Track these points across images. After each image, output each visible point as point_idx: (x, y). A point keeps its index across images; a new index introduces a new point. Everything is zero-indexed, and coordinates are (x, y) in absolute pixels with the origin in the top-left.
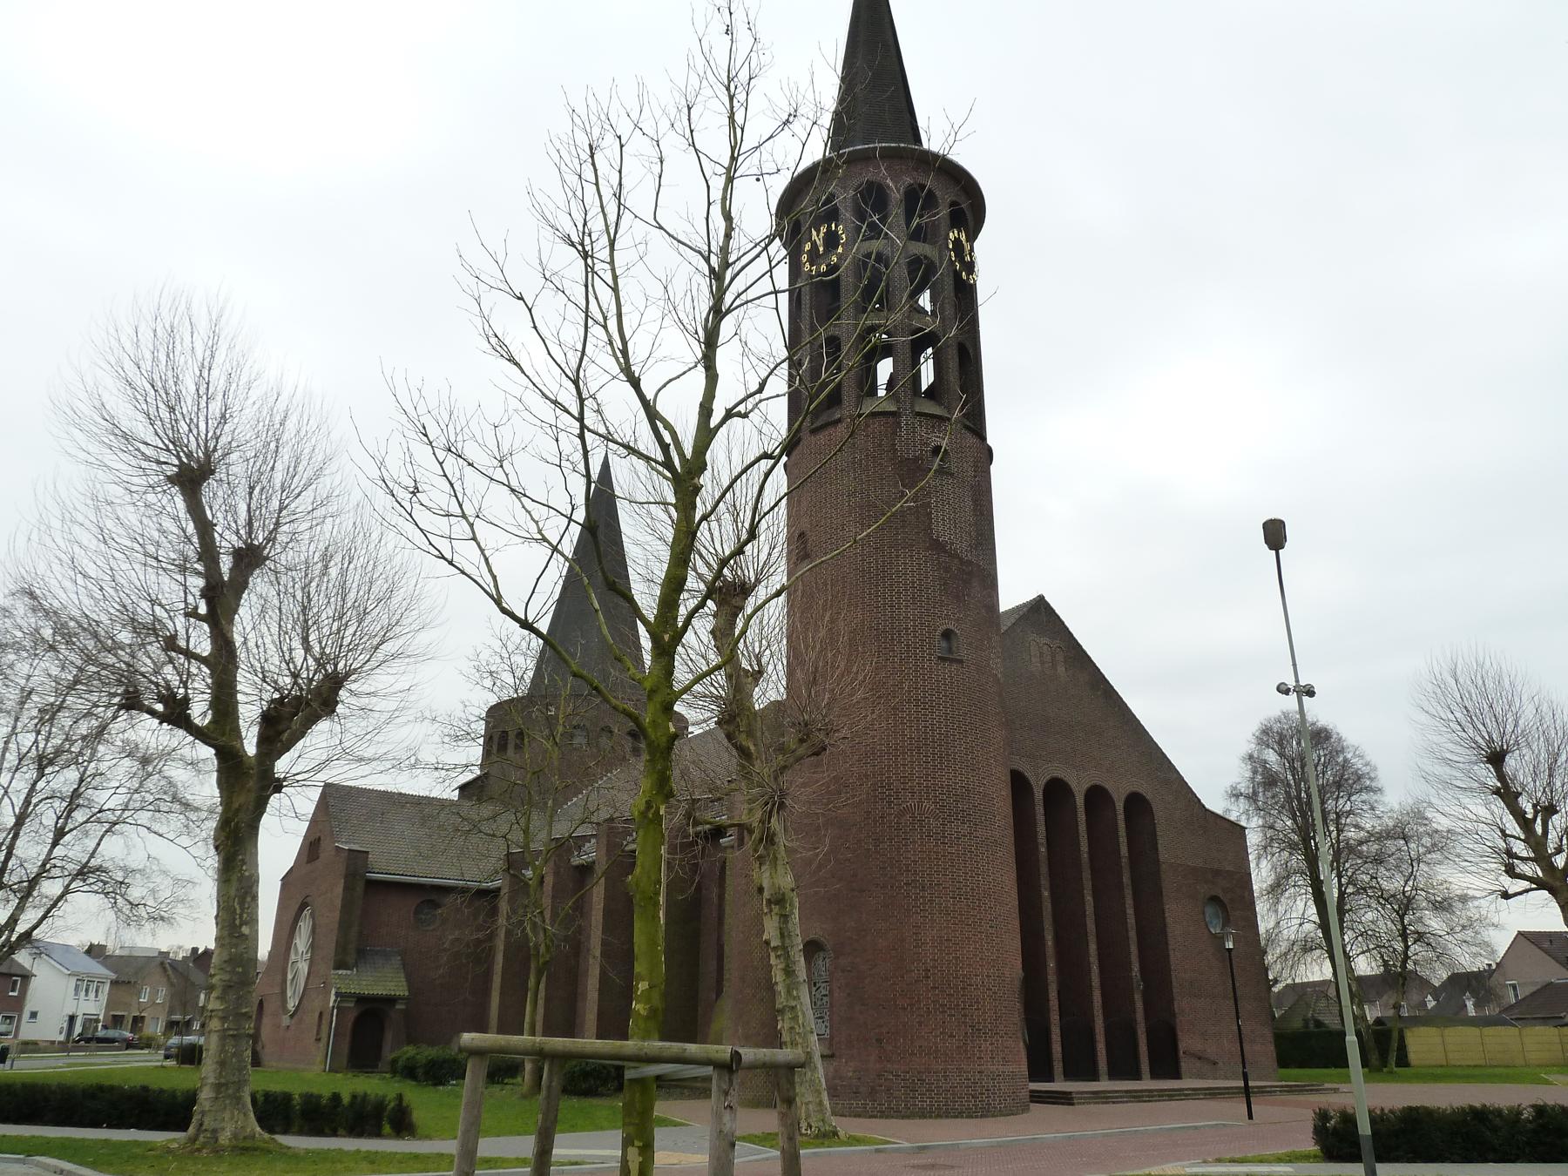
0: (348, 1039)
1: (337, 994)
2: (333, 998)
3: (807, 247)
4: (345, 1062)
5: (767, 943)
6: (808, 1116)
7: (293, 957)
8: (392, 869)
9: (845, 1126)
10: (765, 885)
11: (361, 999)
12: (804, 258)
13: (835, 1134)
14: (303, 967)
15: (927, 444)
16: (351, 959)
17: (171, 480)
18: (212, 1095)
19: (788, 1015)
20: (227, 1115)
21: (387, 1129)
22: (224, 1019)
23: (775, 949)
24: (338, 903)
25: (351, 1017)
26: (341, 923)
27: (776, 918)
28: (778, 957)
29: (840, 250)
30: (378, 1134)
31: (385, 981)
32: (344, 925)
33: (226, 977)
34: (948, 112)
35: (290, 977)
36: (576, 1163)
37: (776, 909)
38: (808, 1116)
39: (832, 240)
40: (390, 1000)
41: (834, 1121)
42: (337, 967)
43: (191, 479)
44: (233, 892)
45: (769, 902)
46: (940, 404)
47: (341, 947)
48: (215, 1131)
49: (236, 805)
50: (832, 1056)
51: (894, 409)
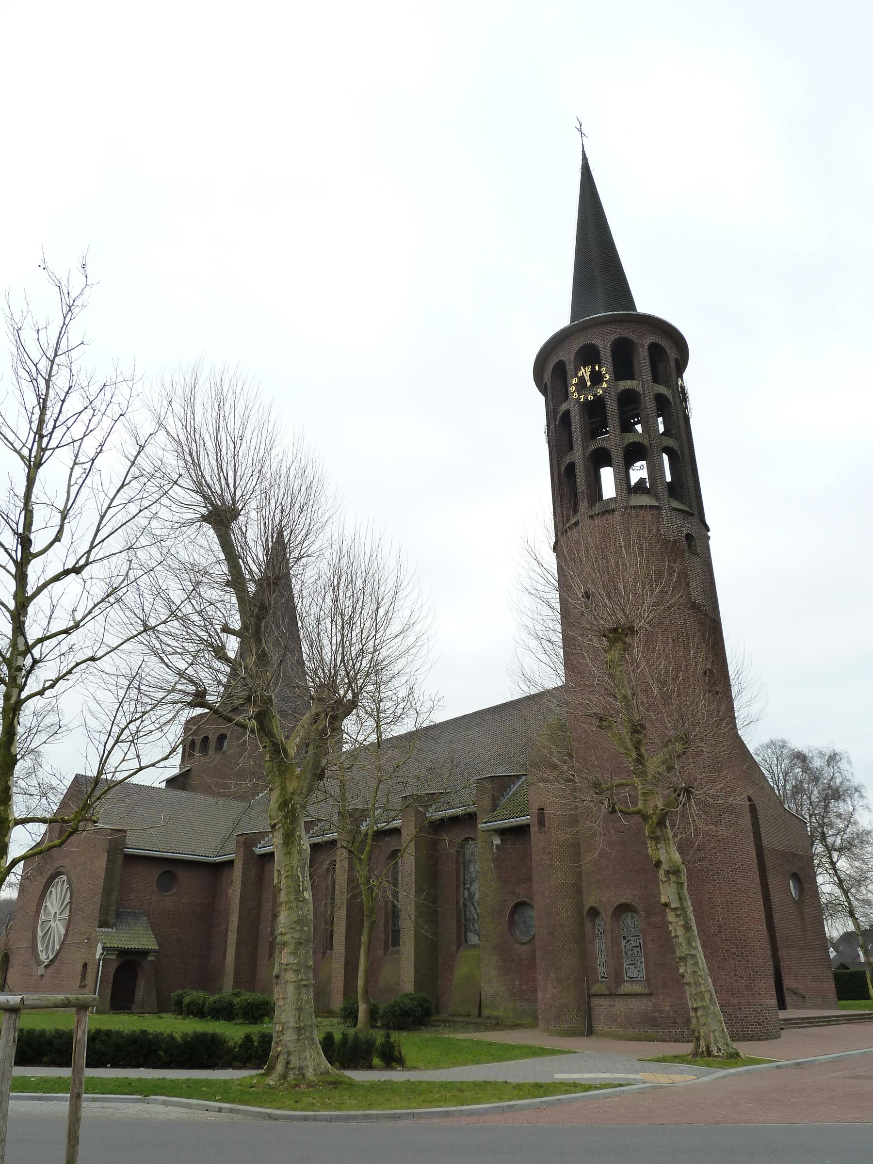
0: (110, 986)
1: (104, 949)
2: (99, 950)
3: (575, 381)
4: (108, 1006)
5: (666, 905)
6: (716, 1042)
7: (43, 917)
8: (141, 845)
9: (745, 1049)
10: (663, 859)
11: (122, 953)
12: (572, 389)
13: (738, 1055)
14: (59, 928)
15: (681, 532)
16: (111, 920)
17: (205, 518)
18: (295, 1037)
19: (690, 961)
20: (307, 1054)
21: (376, 1061)
22: (297, 971)
23: (675, 909)
24: (102, 873)
25: (113, 968)
26: (105, 889)
27: (674, 885)
28: (677, 916)
29: (605, 385)
30: (370, 1067)
31: (138, 937)
32: (107, 891)
33: (297, 935)
34: (651, 294)
35: (40, 934)
36: (621, 1085)
37: (673, 878)
38: (716, 1042)
39: (597, 378)
40: (144, 953)
41: (734, 1045)
42: (101, 926)
43: (221, 517)
44: (295, 863)
45: (667, 873)
46: (683, 503)
47: (104, 909)
48: (301, 1068)
49: (290, 790)
50: (651, 994)
51: (657, 504)
